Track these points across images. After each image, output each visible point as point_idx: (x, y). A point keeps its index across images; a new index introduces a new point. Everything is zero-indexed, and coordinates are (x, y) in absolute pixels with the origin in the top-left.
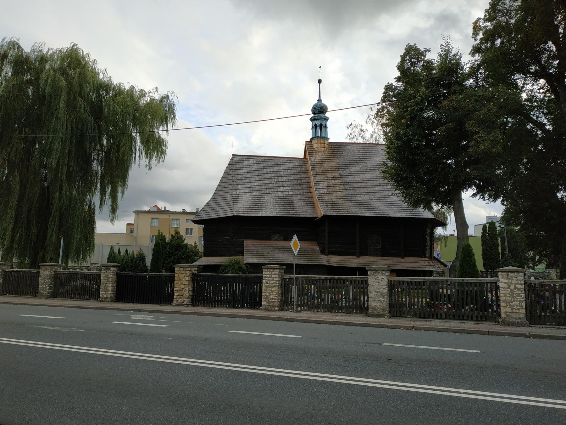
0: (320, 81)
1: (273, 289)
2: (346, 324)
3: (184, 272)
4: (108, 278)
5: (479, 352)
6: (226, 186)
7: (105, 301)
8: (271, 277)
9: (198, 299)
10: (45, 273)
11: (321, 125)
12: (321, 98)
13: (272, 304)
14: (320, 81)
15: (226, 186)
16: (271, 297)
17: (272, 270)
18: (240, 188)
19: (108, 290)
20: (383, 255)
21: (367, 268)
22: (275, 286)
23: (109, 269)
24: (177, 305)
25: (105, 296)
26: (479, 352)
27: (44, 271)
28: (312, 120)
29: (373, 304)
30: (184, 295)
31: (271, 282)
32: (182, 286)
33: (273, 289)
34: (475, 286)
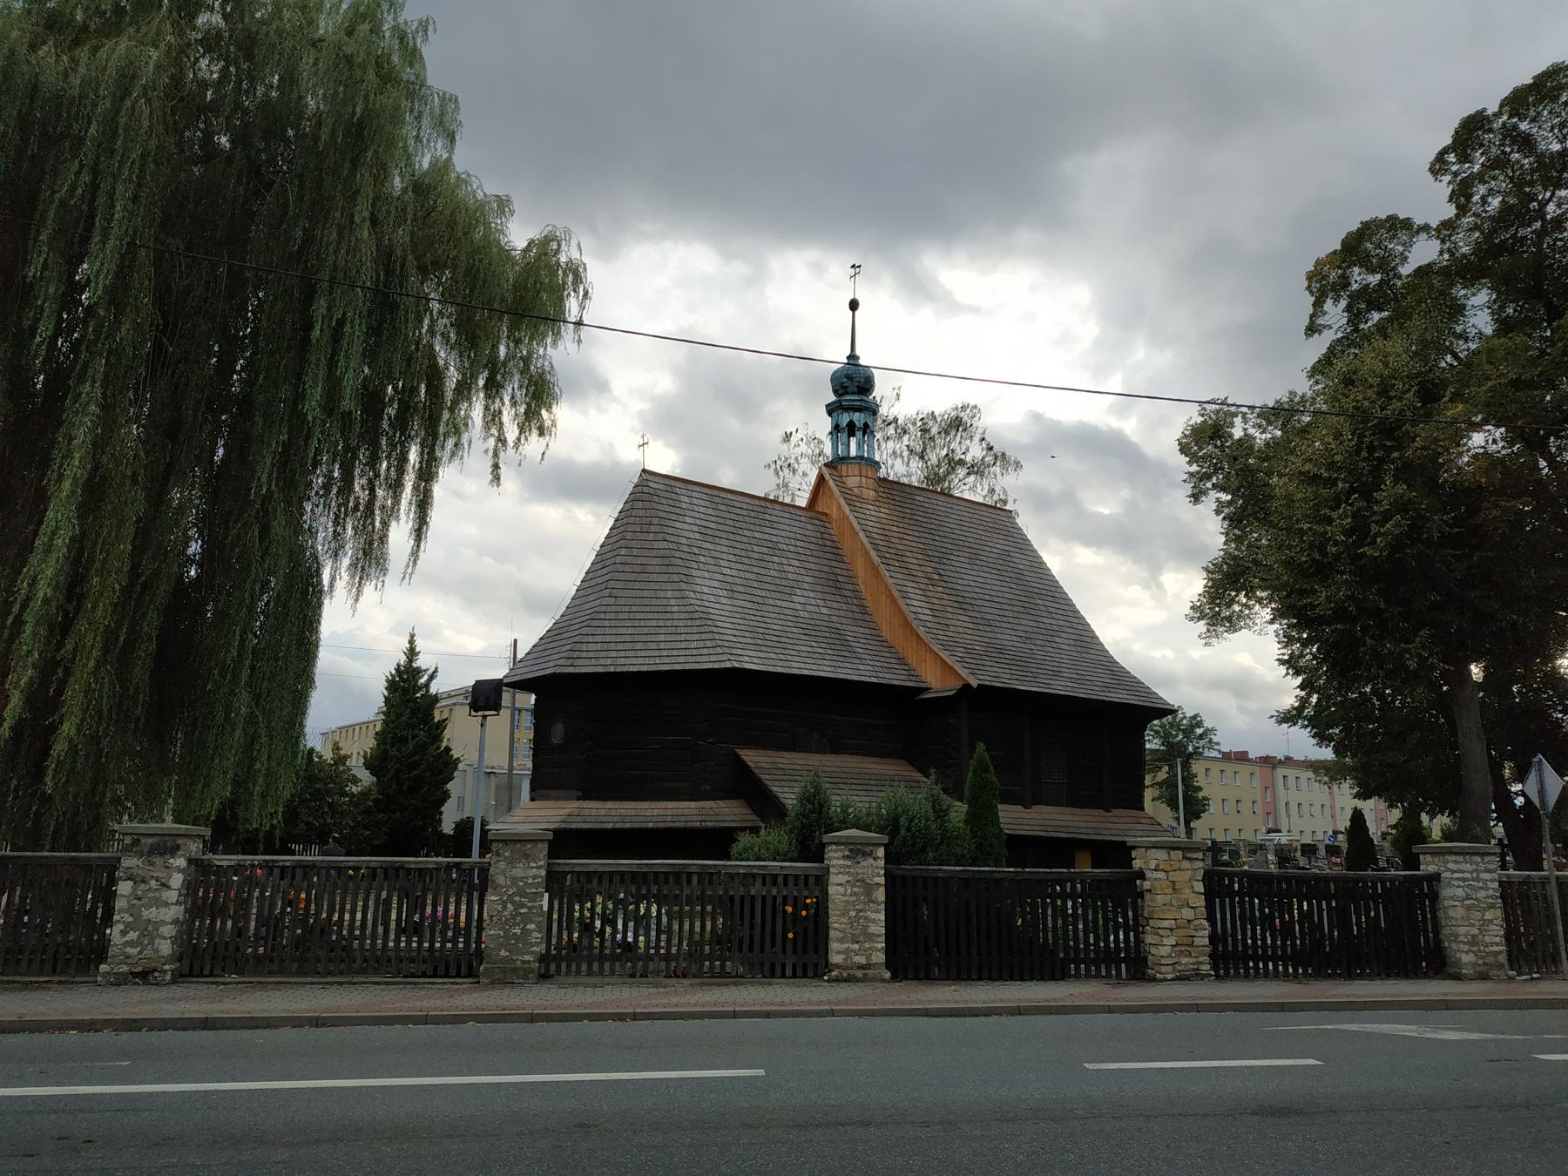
0: (854, 305)
1: (1488, 916)
2: (1018, 1011)
3: (1186, 864)
4: (869, 889)
5: (761, 1072)
6: (649, 569)
7: (865, 979)
8: (1478, 879)
9: (917, 950)
10: (518, 872)
11: (866, 425)
12: (858, 352)
13: (1490, 960)
14: (854, 305)
15: (649, 569)
16: (1487, 939)
17: (1478, 859)
18: (699, 581)
19: (871, 937)
20: (1072, 803)
21: (1130, 840)
22: (1492, 906)
23: (870, 854)
24: (1179, 979)
25: (862, 960)
26: (761, 1072)
27: (511, 862)
28: (831, 410)
29: (1161, 947)
30: (1197, 941)
31: (1482, 894)
32: (1187, 914)
33: (1488, 916)
34: (775, 883)
